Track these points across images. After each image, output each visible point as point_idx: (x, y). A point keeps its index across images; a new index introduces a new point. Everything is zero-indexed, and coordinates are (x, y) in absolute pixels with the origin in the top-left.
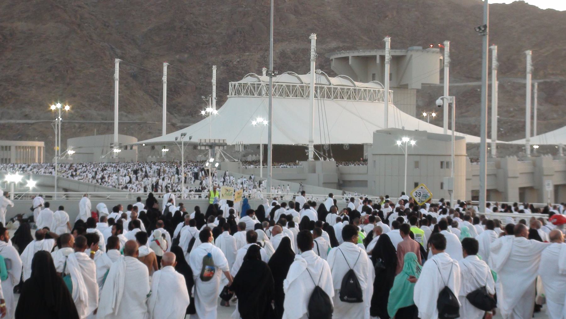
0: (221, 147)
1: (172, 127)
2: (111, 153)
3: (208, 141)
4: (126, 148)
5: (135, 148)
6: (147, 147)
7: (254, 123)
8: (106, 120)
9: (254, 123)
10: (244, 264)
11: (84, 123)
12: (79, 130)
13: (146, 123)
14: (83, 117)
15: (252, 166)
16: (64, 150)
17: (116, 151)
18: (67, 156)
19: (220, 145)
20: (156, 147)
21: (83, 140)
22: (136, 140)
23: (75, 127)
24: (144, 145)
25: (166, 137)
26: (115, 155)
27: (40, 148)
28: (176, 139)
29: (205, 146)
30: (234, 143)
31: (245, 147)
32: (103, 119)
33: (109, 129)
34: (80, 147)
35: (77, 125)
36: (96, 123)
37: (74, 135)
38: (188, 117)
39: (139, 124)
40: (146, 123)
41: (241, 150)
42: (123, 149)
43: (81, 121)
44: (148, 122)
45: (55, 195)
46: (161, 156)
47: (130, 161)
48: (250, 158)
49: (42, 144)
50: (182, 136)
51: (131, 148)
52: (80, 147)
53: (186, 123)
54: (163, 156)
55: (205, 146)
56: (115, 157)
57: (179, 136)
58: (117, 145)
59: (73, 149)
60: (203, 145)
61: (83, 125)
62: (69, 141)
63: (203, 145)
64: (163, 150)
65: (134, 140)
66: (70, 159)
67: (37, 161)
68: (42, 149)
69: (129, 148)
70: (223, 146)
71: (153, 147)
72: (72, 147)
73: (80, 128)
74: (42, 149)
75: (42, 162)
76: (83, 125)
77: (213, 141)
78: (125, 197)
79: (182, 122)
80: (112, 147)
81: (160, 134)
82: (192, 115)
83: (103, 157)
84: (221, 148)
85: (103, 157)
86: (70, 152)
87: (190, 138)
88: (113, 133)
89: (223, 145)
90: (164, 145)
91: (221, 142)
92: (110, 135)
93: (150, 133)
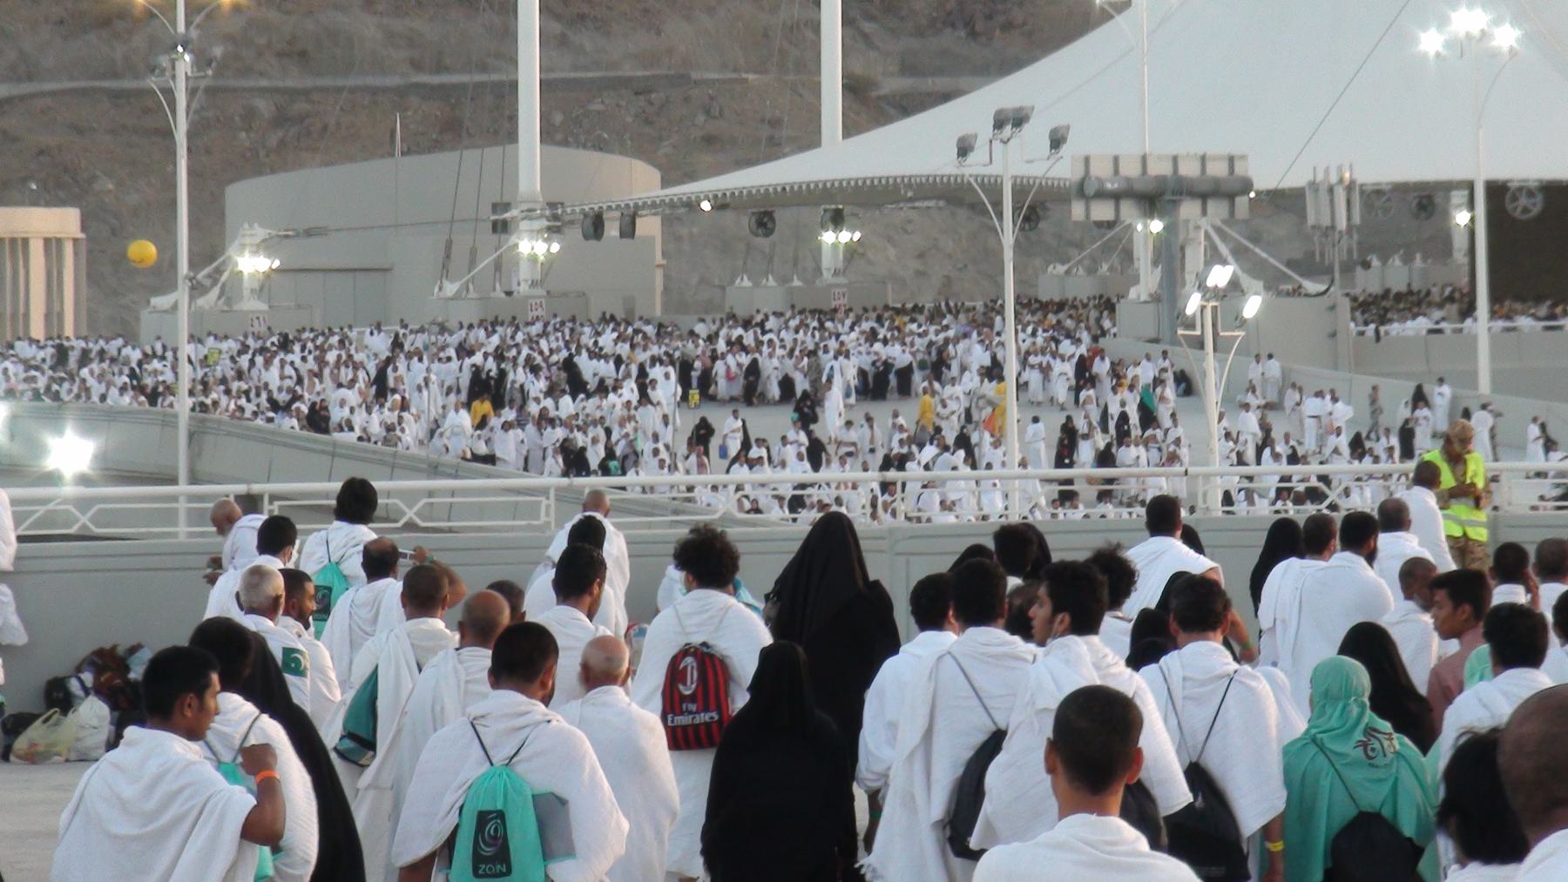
0: (1212, 205)
1: (869, 106)
2: (498, 266)
3: (1130, 170)
4: (596, 225)
5: (649, 226)
6: (729, 217)
7: (1431, 42)
8: (440, 68)
9: (1431, 42)
10: (965, 773)
11: (306, 93)
12: (273, 139)
13: (682, 80)
14: (298, 55)
15: (1422, 324)
16: (209, 250)
17: (532, 246)
18: (231, 291)
19: (1206, 192)
20: (783, 217)
21: (317, 187)
22: (655, 175)
23: (250, 114)
24: (706, 206)
25: (840, 156)
26: (525, 273)
27: (53, 245)
28: (964, 150)
29: (1116, 197)
30: (1296, 179)
31: (1374, 197)
32: (417, 66)
33: (476, 116)
34: (309, 233)
35: (263, 106)
36: (374, 91)
37: (253, 164)
38: (951, 39)
39: (642, 89)
40: (682, 80)
41: (1342, 224)
42: (575, 233)
43: (290, 83)
44: (695, 75)
45: (182, 505)
46: (818, 270)
47: (508, 320)
48: (1395, 274)
49: (64, 221)
50: (999, 124)
51: (628, 231)
52: (309, 233)
53: (939, 72)
54: (827, 275)
55: (1116, 197)
56: (524, 289)
57: (983, 128)
58: (541, 208)
59: (267, 247)
60: (1101, 195)
61: (301, 106)
62: (239, 195)
63: (1101, 195)
64: (828, 237)
65: (638, 180)
66: (252, 305)
67: (37, 330)
68: (68, 249)
69: (612, 230)
70: (1231, 197)
71: (764, 214)
72: (261, 233)
73: (281, 119)
74: (68, 249)
75: (69, 330)
76: (301, 106)
77: (1165, 169)
78: (533, 511)
79: (908, 68)
80: (501, 227)
81: (809, 138)
82: (969, 24)
83: (451, 288)
84: (1218, 209)
85: (451, 288)
86: (251, 264)
87: (1057, 141)
88: (512, 137)
89: (1224, 190)
90: (837, 203)
91: (1218, 170)
92: (493, 153)
93: (710, 140)
